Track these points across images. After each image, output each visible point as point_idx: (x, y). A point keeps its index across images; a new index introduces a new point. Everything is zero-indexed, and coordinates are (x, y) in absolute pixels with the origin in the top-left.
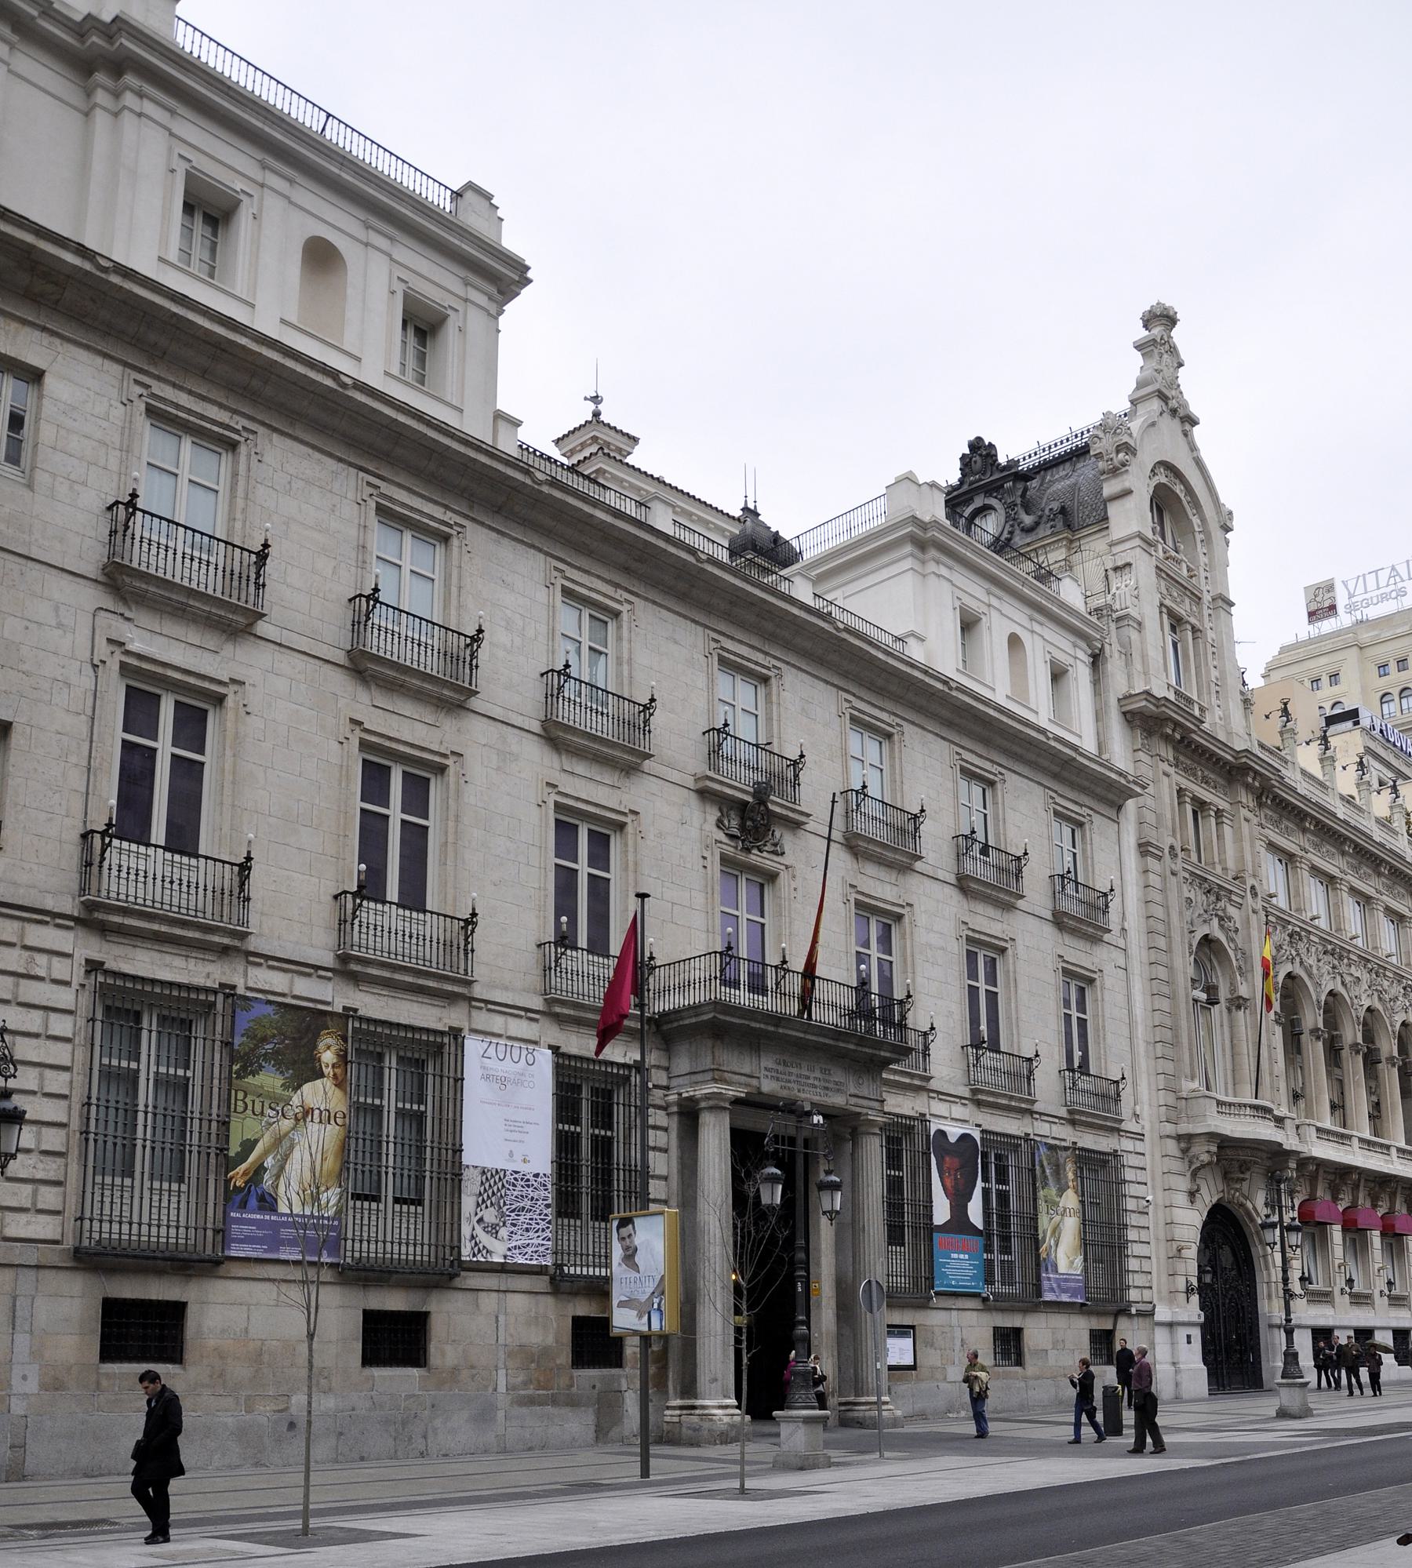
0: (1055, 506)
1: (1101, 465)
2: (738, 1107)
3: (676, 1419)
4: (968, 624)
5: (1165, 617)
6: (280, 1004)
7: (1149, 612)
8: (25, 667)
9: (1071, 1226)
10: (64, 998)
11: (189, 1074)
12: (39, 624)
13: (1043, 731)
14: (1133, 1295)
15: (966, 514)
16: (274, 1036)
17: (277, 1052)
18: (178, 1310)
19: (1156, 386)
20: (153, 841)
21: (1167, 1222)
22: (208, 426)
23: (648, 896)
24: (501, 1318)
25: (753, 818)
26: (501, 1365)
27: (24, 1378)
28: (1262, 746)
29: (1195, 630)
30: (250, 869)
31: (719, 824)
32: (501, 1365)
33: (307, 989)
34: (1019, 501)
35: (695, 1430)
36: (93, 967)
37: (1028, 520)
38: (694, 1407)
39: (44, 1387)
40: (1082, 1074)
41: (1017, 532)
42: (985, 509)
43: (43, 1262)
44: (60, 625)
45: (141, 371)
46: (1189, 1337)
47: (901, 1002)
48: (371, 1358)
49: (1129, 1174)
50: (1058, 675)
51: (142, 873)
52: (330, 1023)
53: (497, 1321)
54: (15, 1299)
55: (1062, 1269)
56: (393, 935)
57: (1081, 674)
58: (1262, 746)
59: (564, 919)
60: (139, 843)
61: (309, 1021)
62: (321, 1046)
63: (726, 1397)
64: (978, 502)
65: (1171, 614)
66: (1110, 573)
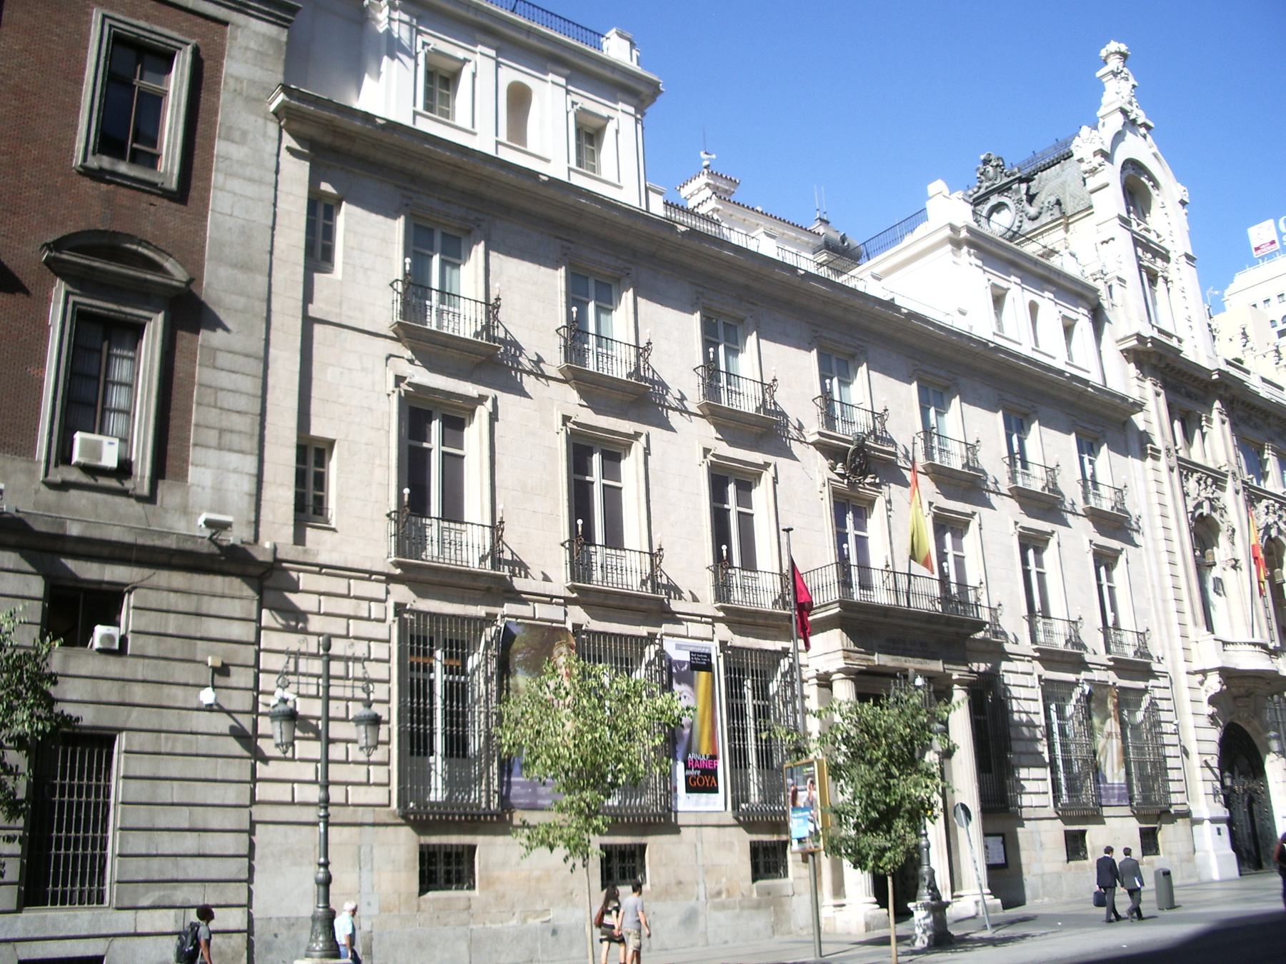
0: (1053, 199)
1: (1084, 167)
4: (998, 300)
5: (1144, 274)
7: (1131, 273)
8: (341, 400)
10: (379, 631)
12: (350, 369)
13: (1061, 372)
14: (1174, 798)
15: (984, 214)
17: (526, 660)
18: (472, 849)
19: (1118, 105)
21: (1194, 737)
22: (261, 7)
24: (699, 846)
25: (862, 468)
27: (369, 904)
28: (1228, 363)
29: (1166, 280)
31: (833, 469)
34: (1024, 197)
36: (400, 609)
37: (1032, 211)
39: (382, 910)
41: (1026, 220)
42: (999, 207)
43: (378, 821)
44: (363, 369)
45: (405, 189)
46: (1219, 829)
50: (1068, 329)
54: (360, 848)
57: (1084, 325)
58: (1228, 363)
62: (556, 653)
64: (994, 200)
65: (1148, 270)
66: (1099, 245)
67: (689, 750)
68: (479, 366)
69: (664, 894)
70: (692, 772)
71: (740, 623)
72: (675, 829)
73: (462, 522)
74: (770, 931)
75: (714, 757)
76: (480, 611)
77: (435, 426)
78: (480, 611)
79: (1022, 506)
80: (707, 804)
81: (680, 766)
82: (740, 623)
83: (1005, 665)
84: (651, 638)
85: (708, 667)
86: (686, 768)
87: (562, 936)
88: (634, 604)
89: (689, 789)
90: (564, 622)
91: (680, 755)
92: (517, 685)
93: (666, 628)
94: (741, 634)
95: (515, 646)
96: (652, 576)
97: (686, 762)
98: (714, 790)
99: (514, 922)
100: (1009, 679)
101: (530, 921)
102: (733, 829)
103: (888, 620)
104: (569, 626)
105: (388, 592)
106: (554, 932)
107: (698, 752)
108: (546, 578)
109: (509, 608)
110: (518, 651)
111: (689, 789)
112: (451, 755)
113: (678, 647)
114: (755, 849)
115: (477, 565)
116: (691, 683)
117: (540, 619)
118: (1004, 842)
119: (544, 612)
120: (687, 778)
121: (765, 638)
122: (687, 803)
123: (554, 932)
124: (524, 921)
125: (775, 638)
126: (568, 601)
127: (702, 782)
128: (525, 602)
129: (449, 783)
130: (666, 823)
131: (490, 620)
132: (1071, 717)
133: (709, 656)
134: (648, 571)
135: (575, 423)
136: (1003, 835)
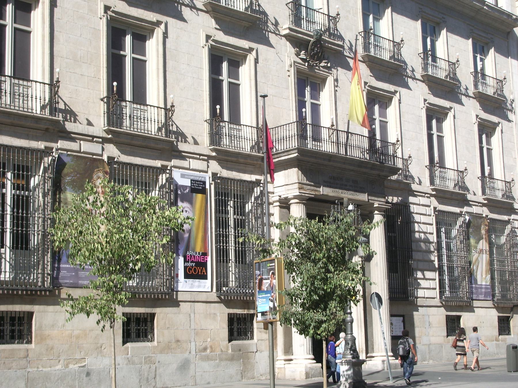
2: (311, 202)
3: (283, 366)
6: (77, 156)
9: (485, 258)
11: (13, 192)
16: (71, 173)
17: (73, 181)
20: (6, 74)
23: (267, 96)
26: (192, 340)
30: (59, 87)
32: (192, 340)
33: (94, 148)
35: (293, 372)
38: (291, 360)
40: (440, 167)
47: (394, 144)
48: (509, 333)
49: (417, 218)
51: (146, 119)
52: (99, 165)
53: (190, 317)
55: (479, 283)
56: (153, 122)
59: (115, 84)
60: (140, 104)
61: (91, 164)
62: (95, 177)
63: (382, 352)
67: (187, 249)
68: (248, 29)
69: (167, 348)
70: (189, 264)
71: (227, 161)
72: (176, 303)
73: (28, 80)
74: (239, 377)
75: (205, 254)
76: (41, 145)
77: (128, 39)
78: (41, 145)
79: (430, 88)
80: (199, 286)
81: (181, 260)
82: (227, 161)
83: (411, 199)
84: (163, 169)
85: (203, 191)
86: (185, 261)
87: (94, 377)
88: (153, 145)
89: (187, 276)
90: (102, 155)
91: (181, 252)
92: (66, 199)
93: (174, 162)
94: (228, 169)
95: (65, 171)
96: (166, 125)
97: (185, 257)
98: (205, 277)
99: (59, 367)
100: (414, 209)
101: (71, 366)
102: (216, 305)
103: (331, 163)
104: (105, 158)
105: (103, 149)
106: (88, 374)
107: (194, 250)
108: (90, 124)
109: (61, 144)
110: (68, 175)
111: (187, 276)
112: (17, 248)
113: (183, 176)
114: (232, 320)
115: (38, 112)
116: (191, 202)
117: (84, 153)
118: (404, 321)
119: (86, 147)
120: (185, 268)
121: (244, 172)
122: (184, 285)
123: (88, 374)
124: (67, 366)
125: (251, 173)
126: (105, 141)
127: (196, 271)
128: (73, 140)
129: (14, 268)
130: (169, 299)
131: (48, 151)
132: (34, 188)
133: (204, 183)
134: (163, 121)
135: (113, 12)
136: (403, 316)
